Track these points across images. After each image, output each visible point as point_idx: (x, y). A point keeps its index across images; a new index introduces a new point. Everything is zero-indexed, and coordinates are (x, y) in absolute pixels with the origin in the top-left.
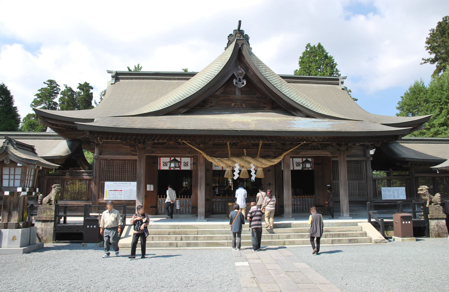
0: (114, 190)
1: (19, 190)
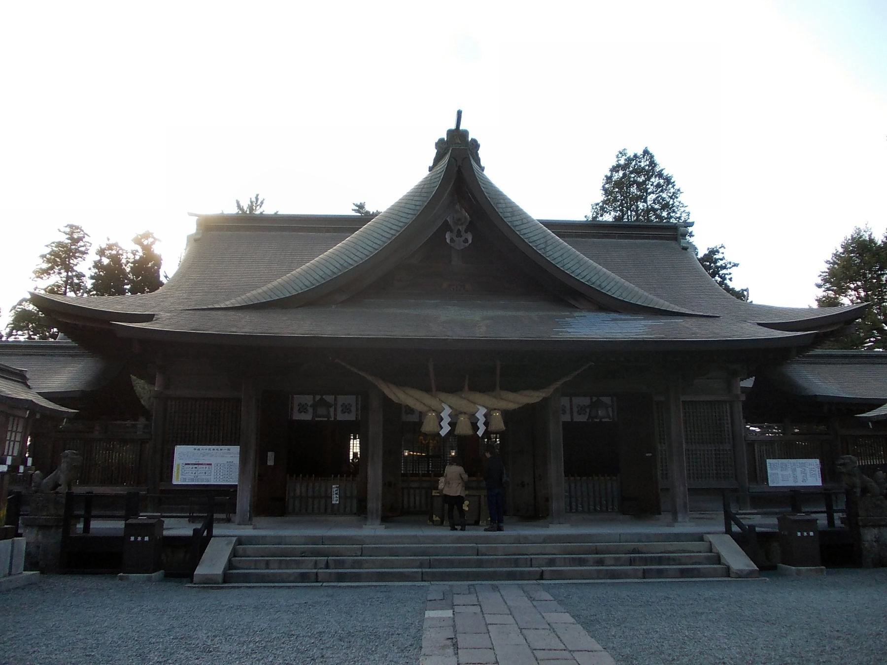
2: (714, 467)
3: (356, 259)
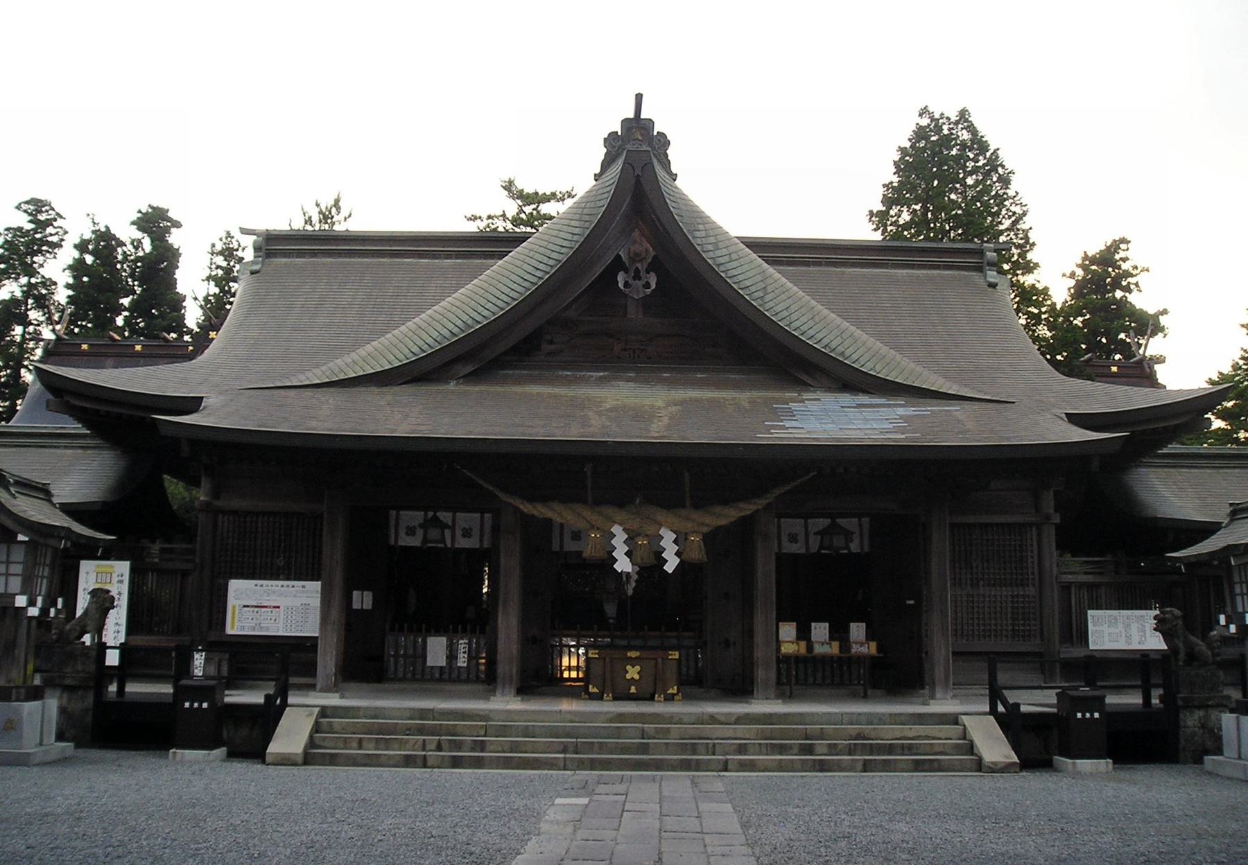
1: (21, 601)
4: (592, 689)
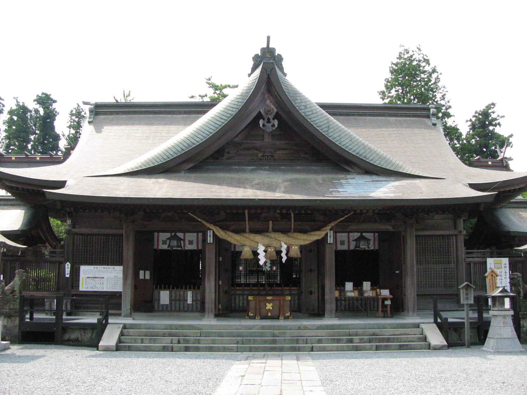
0: (93, 278)
2: (443, 280)
3: (198, 139)
4: (251, 314)
